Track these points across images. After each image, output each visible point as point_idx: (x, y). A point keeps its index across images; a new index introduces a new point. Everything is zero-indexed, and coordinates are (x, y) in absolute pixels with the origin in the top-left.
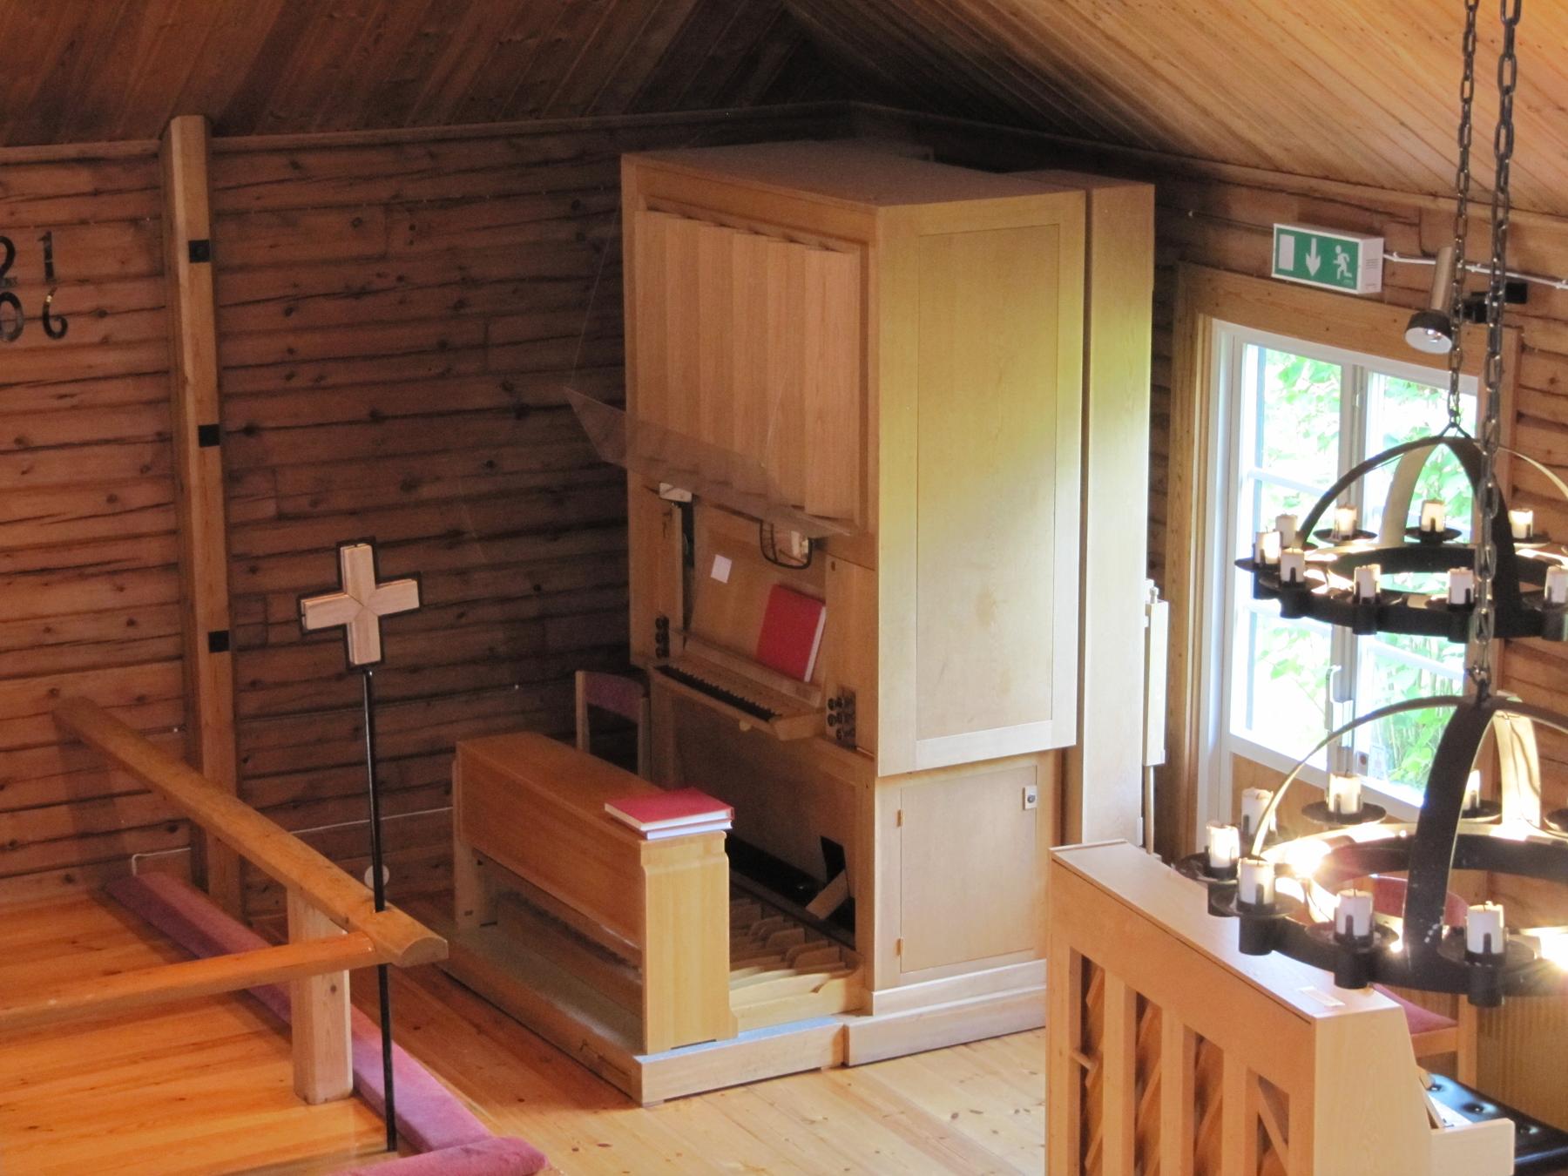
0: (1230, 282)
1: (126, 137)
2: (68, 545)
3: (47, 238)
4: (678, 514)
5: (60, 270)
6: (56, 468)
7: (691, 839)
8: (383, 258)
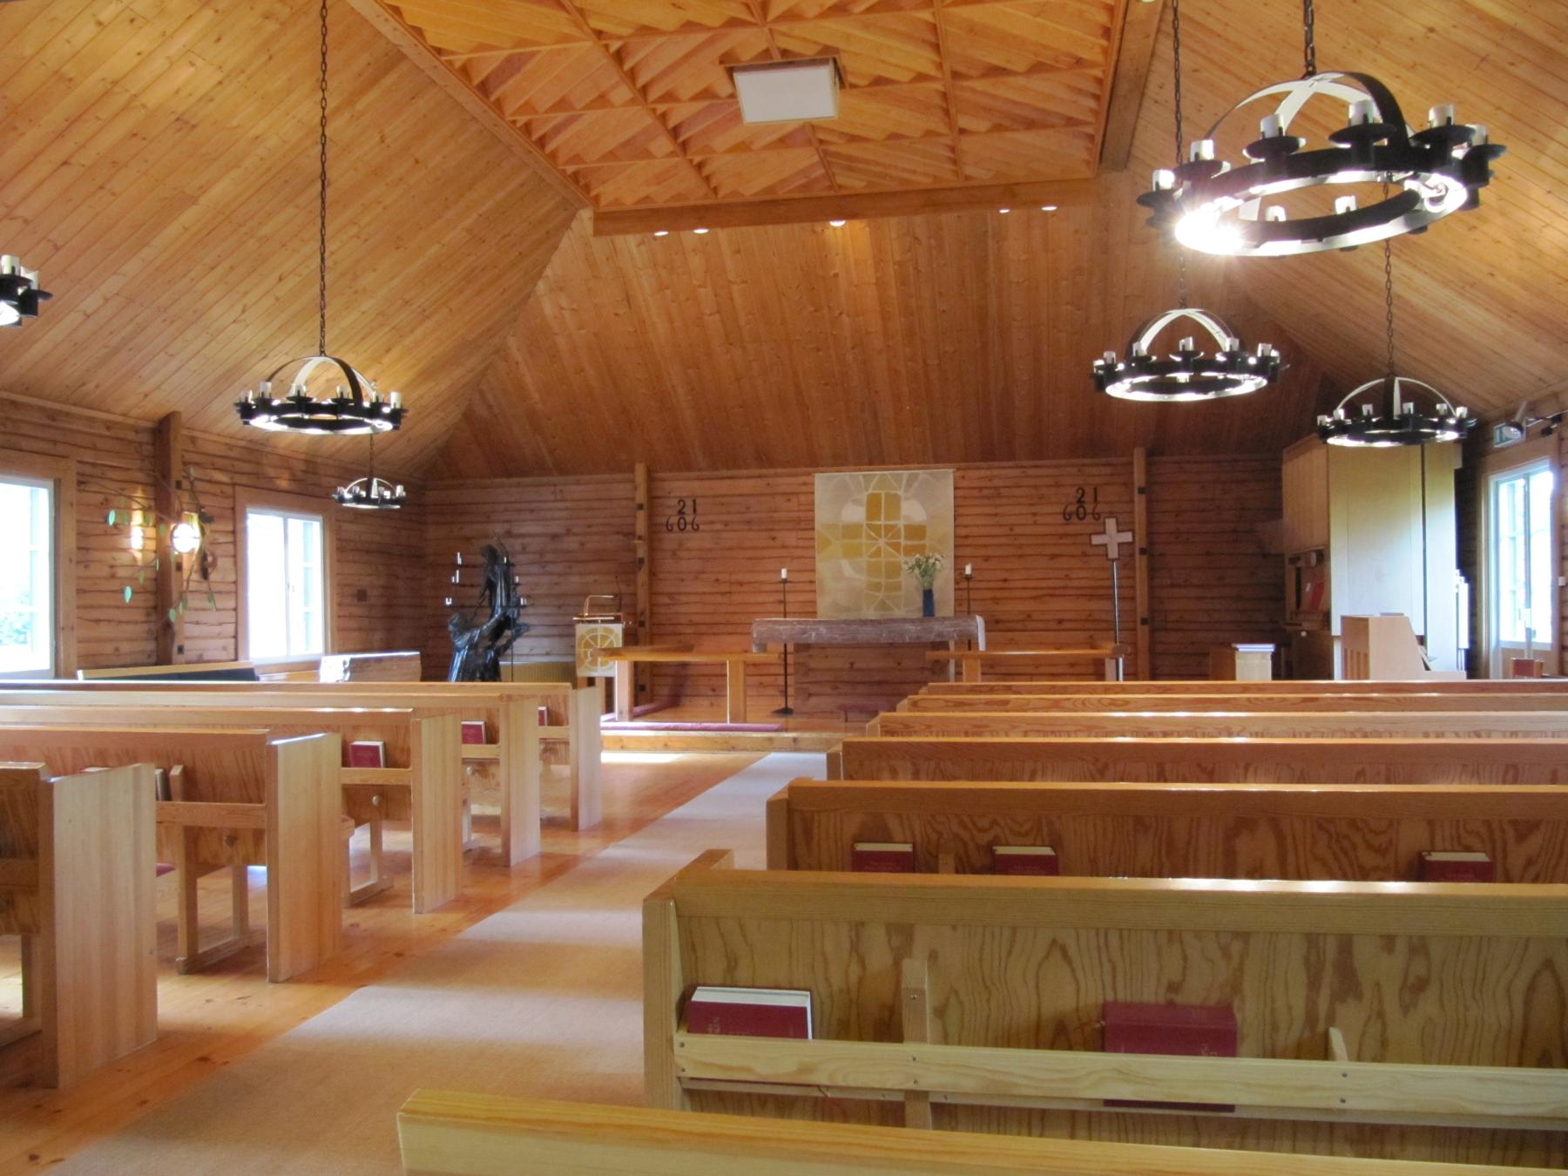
2: (1098, 588)
5: (1099, 499)
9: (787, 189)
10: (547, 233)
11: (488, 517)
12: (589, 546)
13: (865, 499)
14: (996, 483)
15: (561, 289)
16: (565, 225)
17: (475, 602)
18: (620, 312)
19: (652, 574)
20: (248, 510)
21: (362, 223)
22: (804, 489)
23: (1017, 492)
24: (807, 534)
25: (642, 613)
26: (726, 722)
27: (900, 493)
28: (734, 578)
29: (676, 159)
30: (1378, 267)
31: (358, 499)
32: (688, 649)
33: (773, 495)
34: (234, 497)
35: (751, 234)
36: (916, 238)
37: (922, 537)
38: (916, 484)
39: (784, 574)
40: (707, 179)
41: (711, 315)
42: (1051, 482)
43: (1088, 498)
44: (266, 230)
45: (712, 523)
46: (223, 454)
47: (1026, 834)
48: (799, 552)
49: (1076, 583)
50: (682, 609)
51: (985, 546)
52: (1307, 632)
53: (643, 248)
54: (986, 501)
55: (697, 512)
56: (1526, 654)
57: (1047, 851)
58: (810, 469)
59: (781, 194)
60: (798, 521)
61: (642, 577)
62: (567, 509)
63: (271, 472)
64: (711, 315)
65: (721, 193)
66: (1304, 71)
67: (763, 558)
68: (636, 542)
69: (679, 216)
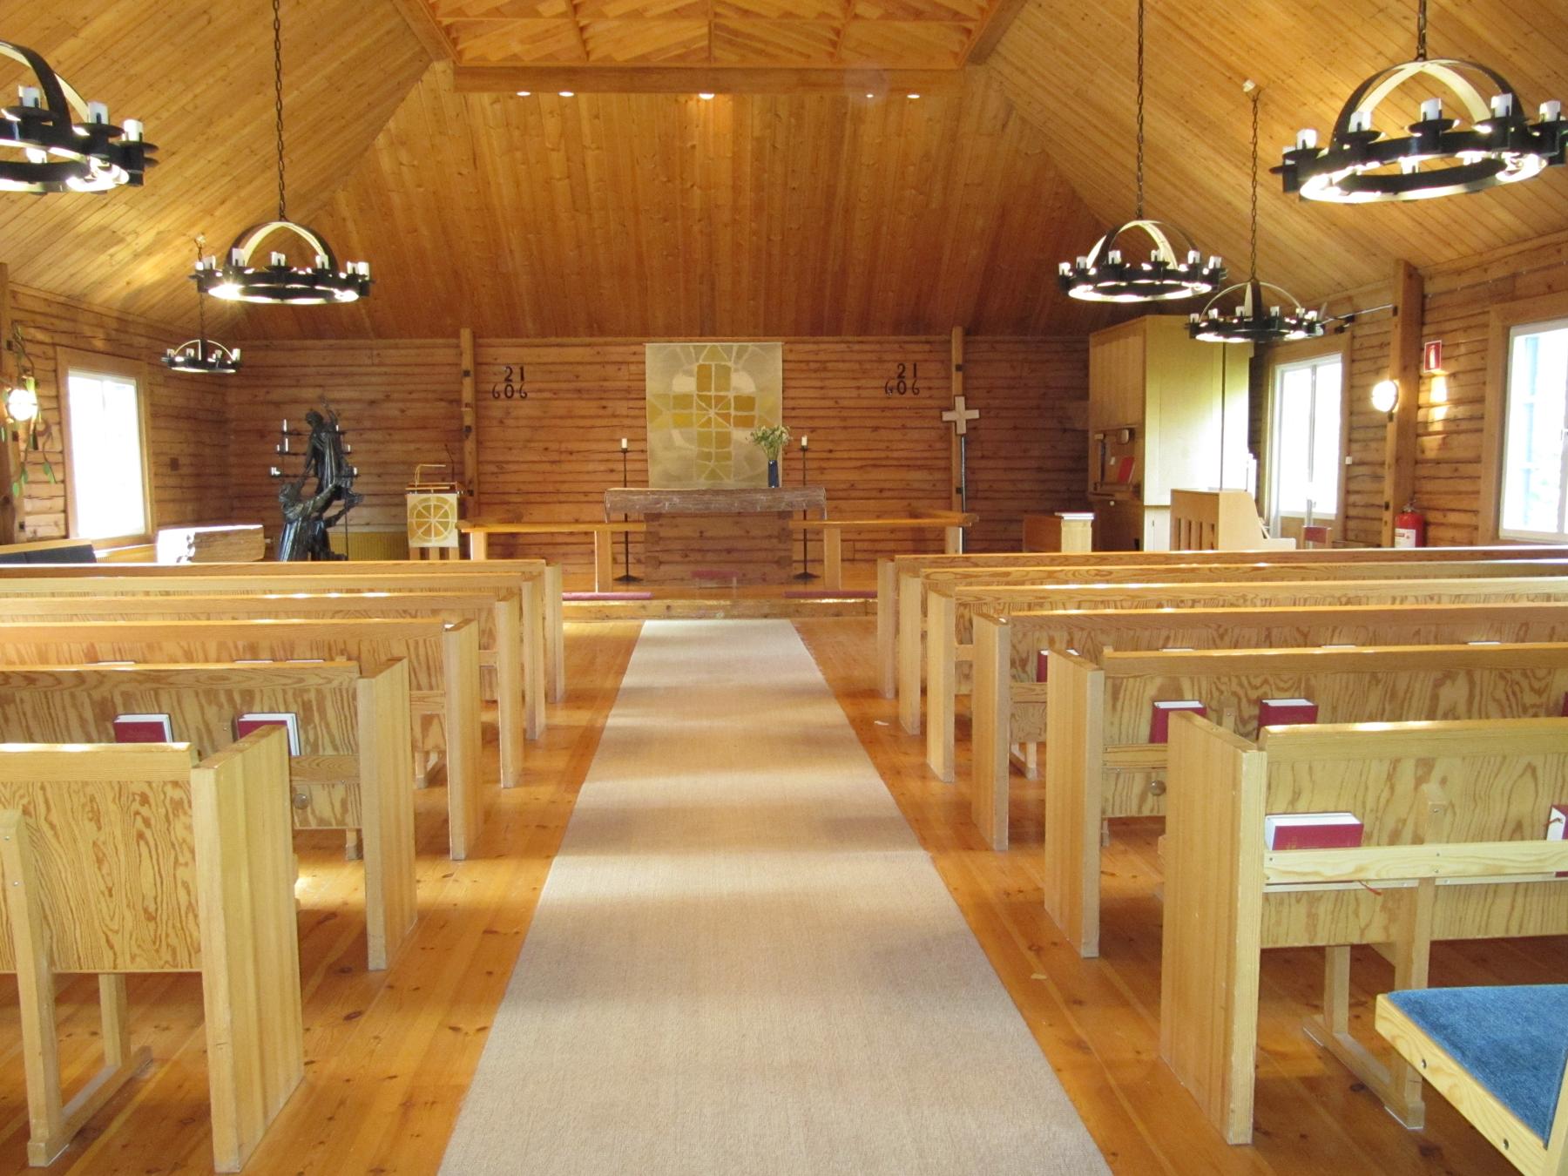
0: (1279, 350)
1: (940, 334)
3: (915, 365)
4: (1100, 444)
5: (919, 374)
6: (915, 435)
7: (1080, 521)
8: (1020, 377)
9: (662, 57)
10: (399, 83)
11: (298, 381)
12: (410, 413)
13: (696, 369)
14: (823, 357)
15: (403, 143)
16: (417, 77)
17: (301, 471)
18: (465, 172)
19: (479, 443)
20: (70, 372)
21: (231, 65)
22: (634, 359)
23: (841, 365)
24: (639, 404)
25: (470, 482)
26: (594, 591)
27: (730, 364)
28: (564, 447)
29: (565, 20)
30: (1262, 185)
31: (192, 362)
32: (517, 519)
33: (603, 364)
34: (55, 359)
35: (614, 101)
36: (777, 115)
37: (752, 409)
38: (745, 357)
39: (624, 444)
40: (585, 42)
41: (560, 179)
42: (873, 357)
43: (909, 373)
44: (138, 69)
45: (540, 391)
46: (42, 310)
47: (1286, 690)
48: (627, 422)
49: (895, 455)
50: (508, 478)
51: (812, 418)
52: (1115, 502)
53: (497, 106)
54: (813, 375)
55: (526, 380)
56: (1306, 521)
57: (1303, 702)
58: (640, 339)
59: (655, 61)
60: (628, 390)
61: (469, 445)
62: (386, 374)
63: (87, 331)
64: (560, 179)
65: (592, 58)
66: (1415, 55)
67: (592, 427)
68: (464, 409)
69: (544, 76)
